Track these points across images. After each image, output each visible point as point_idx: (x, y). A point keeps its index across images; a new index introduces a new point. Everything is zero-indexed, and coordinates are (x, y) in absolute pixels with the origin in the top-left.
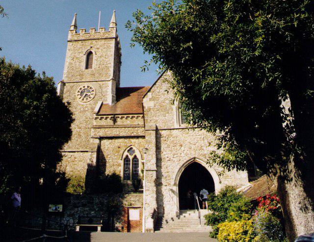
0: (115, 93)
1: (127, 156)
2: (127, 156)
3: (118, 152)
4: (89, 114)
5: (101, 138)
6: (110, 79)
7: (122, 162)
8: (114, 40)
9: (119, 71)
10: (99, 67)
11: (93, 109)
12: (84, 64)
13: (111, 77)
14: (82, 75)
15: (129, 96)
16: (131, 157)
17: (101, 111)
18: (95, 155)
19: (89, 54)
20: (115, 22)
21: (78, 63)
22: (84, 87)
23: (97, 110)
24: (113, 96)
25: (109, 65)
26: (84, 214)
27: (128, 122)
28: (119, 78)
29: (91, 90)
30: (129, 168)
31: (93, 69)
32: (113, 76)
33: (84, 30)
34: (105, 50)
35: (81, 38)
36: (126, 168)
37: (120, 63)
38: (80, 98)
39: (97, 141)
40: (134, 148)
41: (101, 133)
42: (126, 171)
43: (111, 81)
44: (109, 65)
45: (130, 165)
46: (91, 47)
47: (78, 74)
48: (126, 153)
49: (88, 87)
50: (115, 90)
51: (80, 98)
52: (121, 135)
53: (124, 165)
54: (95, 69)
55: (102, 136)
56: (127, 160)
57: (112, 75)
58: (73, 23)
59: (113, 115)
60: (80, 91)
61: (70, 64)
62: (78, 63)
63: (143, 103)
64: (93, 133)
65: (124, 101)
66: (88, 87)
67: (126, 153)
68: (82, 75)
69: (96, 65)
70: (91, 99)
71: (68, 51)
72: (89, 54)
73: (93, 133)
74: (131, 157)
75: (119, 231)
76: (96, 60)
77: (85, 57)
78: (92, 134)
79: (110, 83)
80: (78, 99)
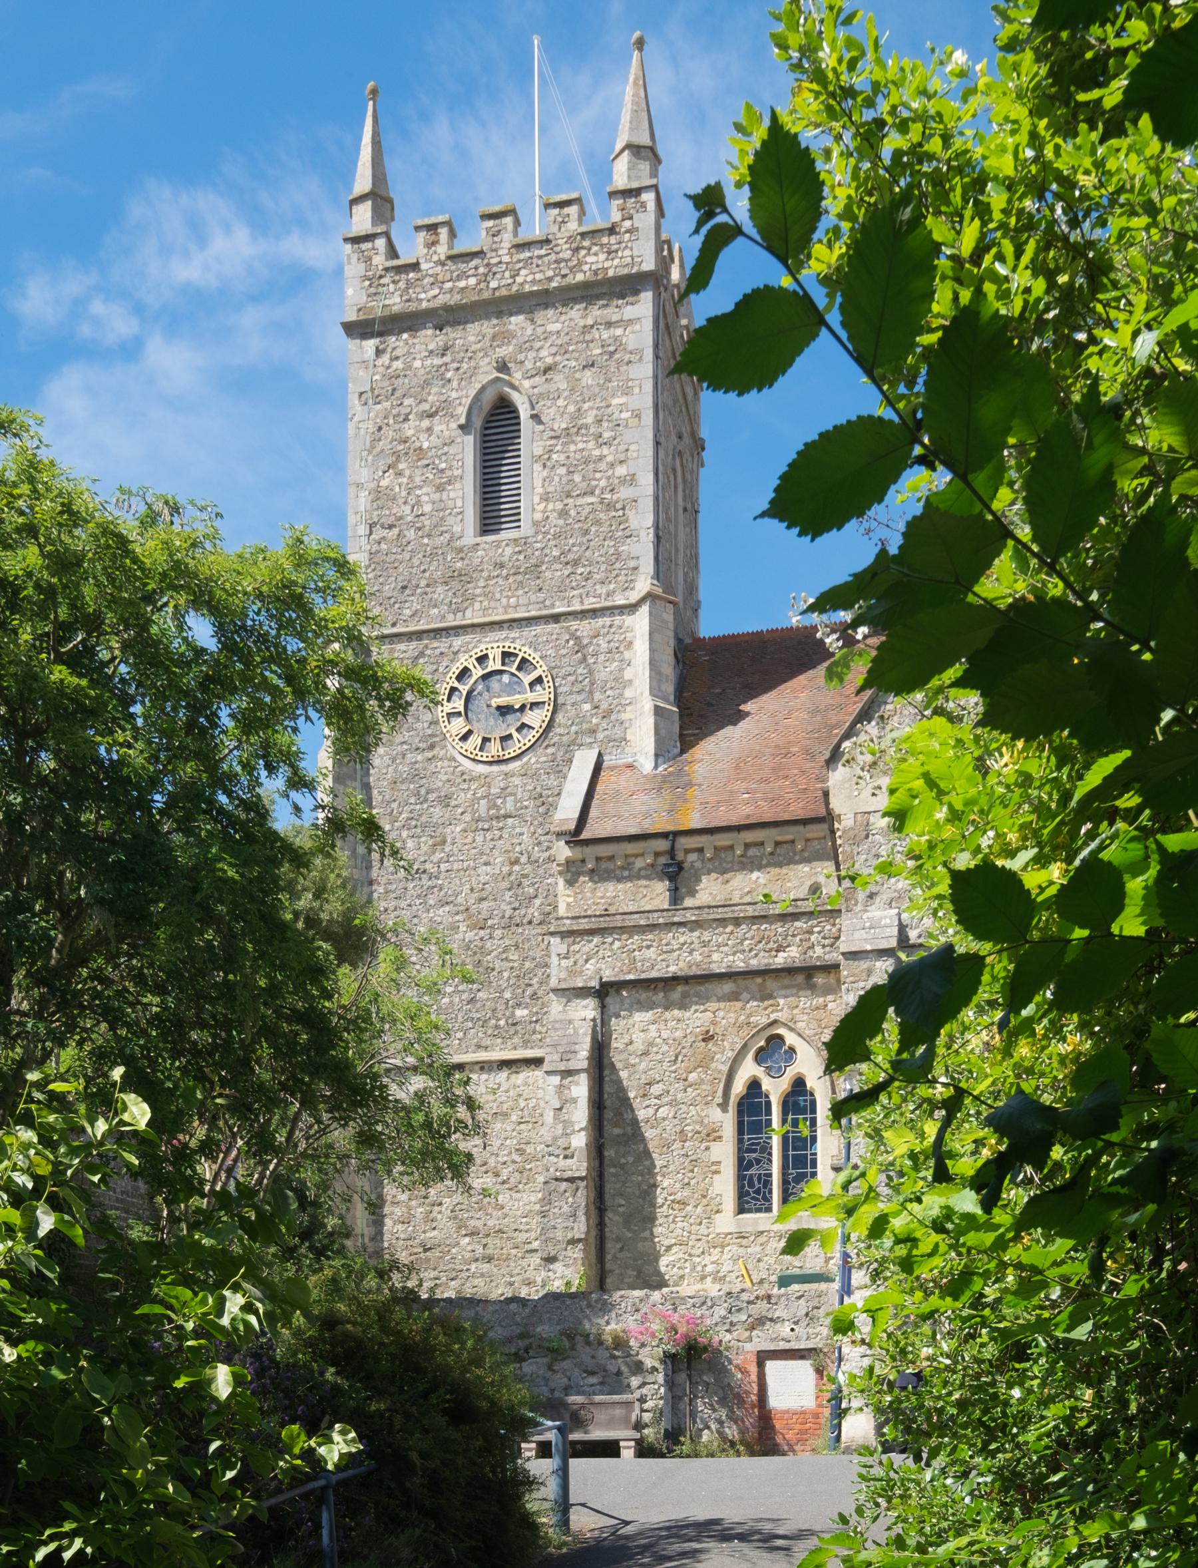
0: (670, 688)
1: (754, 1086)
2: (754, 1086)
3: (704, 1063)
4: (524, 836)
5: (604, 992)
6: (634, 597)
7: (727, 1122)
8: (647, 297)
9: (692, 512)
10: (564, 513)
11: (546, 802)
12: (464, 495)
13: (644, 584)
14: (463, 577)
15: (806, 444)
16: (775, 1089)
17: (594, 812)
18: (581, 1089)
19: (497, 425)
20: (645, 140)
21: (426, 494)
22: (482, 659)
23: (568, 810)
24: (658, 711)
25: (624, 493)
26: (552, 1391)
27: (747, 886)
28: (693, 561)
29: (527, 679)
30: (766, 1149)
31: (526, 529)
32: (657, 575)
33: (444, 232)
34: (588, 378)
35: (428, 298)
36: (749, 1151)
37: (699, 445)
38: (465, 738)
39: (587, 1010)
40: (790, 1039)
41: (605, 962)
42: (750, 1165)
43: (645, 609)
44: (624, 493)
45: (769, 1112)
46: (503, 367)
47: (436, 570)
48: (749, 1069)
49: (506, 655)
50: (668, 668)
51: (465, 738)
52: (720, 962)
53: (740, 1131)
54: (536, 524)
55: (609, 975)
56: (751, 1105)
57: (647, 565)
58: (363, 182)
59: (664, 835)
60: (464, 689)
61: (379, 495)
62: (426, 494)
63: (826, 794)
64: (564, 963)
65: (719, 750)
66: (506, 655)
67: (749, 1069)
68: (463, 577)
69: (546, 498)
70: (531, 736)
71: (354, 401)
72: (497, 425)
73: (564, 963)
74: (775, 1089)
75: (1183, 301)
76: (545, 461)
77: (467, 450)
78: (557, 972)
79: (640, 622)
80: (454, 748)
